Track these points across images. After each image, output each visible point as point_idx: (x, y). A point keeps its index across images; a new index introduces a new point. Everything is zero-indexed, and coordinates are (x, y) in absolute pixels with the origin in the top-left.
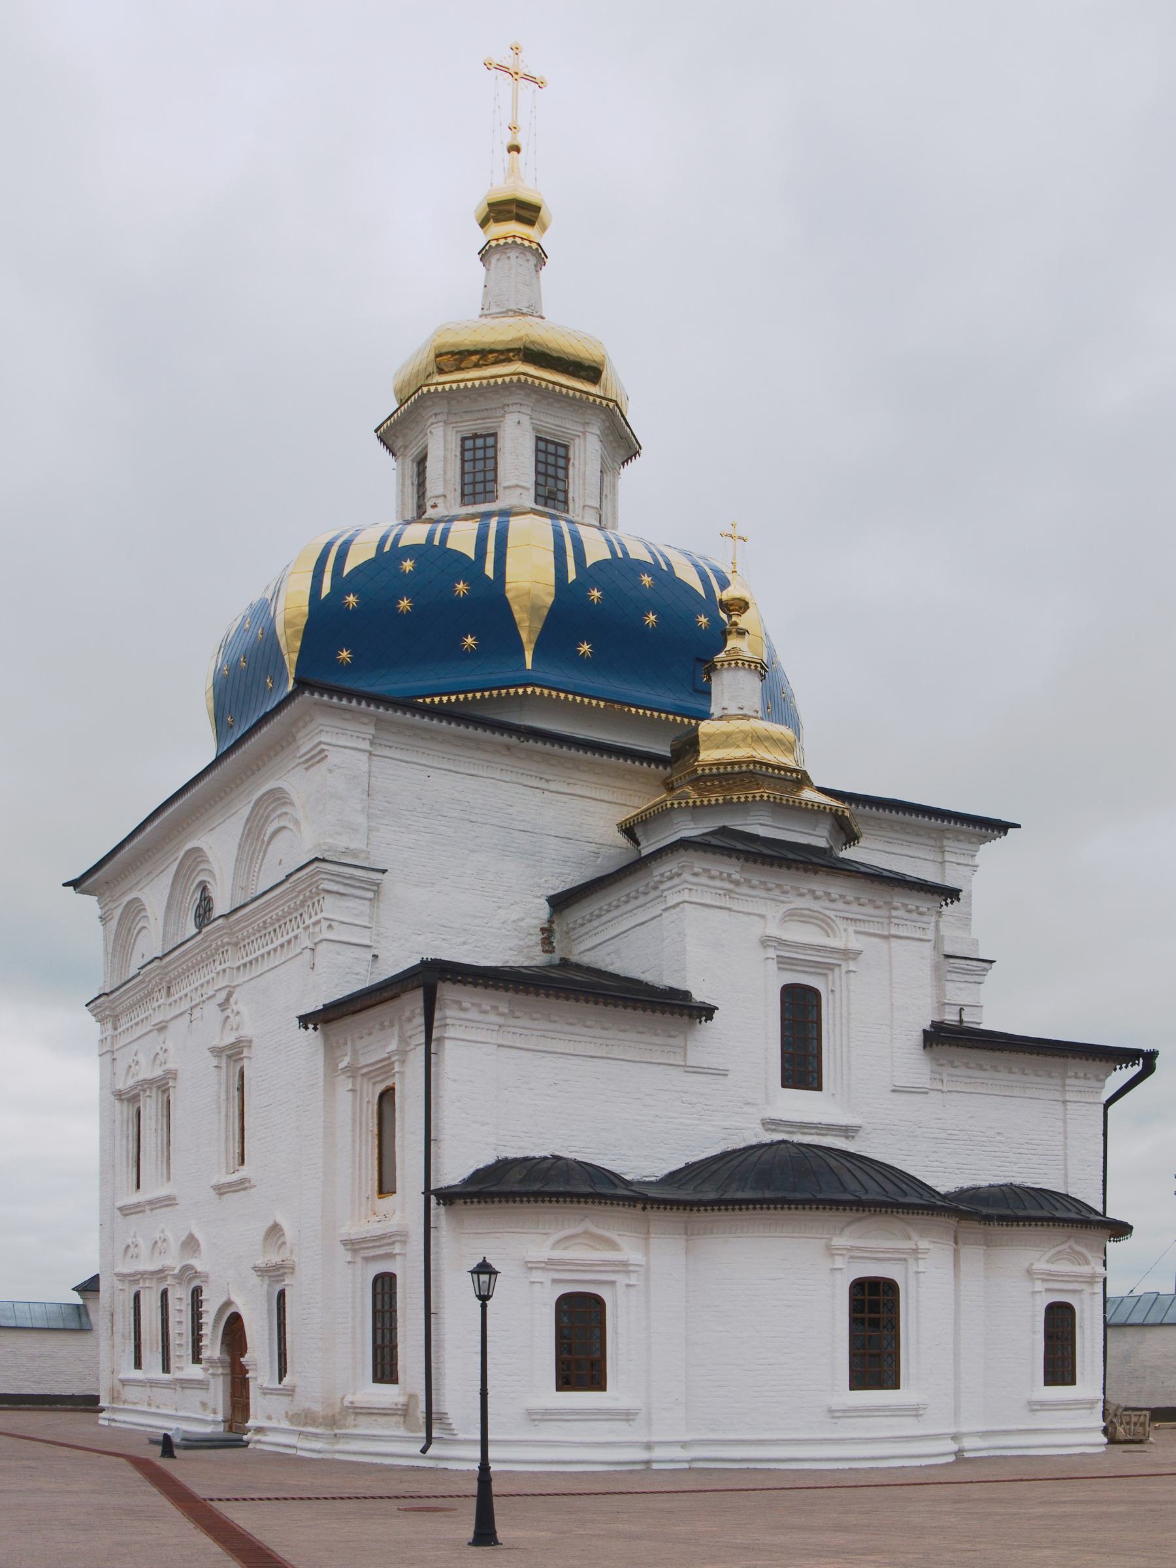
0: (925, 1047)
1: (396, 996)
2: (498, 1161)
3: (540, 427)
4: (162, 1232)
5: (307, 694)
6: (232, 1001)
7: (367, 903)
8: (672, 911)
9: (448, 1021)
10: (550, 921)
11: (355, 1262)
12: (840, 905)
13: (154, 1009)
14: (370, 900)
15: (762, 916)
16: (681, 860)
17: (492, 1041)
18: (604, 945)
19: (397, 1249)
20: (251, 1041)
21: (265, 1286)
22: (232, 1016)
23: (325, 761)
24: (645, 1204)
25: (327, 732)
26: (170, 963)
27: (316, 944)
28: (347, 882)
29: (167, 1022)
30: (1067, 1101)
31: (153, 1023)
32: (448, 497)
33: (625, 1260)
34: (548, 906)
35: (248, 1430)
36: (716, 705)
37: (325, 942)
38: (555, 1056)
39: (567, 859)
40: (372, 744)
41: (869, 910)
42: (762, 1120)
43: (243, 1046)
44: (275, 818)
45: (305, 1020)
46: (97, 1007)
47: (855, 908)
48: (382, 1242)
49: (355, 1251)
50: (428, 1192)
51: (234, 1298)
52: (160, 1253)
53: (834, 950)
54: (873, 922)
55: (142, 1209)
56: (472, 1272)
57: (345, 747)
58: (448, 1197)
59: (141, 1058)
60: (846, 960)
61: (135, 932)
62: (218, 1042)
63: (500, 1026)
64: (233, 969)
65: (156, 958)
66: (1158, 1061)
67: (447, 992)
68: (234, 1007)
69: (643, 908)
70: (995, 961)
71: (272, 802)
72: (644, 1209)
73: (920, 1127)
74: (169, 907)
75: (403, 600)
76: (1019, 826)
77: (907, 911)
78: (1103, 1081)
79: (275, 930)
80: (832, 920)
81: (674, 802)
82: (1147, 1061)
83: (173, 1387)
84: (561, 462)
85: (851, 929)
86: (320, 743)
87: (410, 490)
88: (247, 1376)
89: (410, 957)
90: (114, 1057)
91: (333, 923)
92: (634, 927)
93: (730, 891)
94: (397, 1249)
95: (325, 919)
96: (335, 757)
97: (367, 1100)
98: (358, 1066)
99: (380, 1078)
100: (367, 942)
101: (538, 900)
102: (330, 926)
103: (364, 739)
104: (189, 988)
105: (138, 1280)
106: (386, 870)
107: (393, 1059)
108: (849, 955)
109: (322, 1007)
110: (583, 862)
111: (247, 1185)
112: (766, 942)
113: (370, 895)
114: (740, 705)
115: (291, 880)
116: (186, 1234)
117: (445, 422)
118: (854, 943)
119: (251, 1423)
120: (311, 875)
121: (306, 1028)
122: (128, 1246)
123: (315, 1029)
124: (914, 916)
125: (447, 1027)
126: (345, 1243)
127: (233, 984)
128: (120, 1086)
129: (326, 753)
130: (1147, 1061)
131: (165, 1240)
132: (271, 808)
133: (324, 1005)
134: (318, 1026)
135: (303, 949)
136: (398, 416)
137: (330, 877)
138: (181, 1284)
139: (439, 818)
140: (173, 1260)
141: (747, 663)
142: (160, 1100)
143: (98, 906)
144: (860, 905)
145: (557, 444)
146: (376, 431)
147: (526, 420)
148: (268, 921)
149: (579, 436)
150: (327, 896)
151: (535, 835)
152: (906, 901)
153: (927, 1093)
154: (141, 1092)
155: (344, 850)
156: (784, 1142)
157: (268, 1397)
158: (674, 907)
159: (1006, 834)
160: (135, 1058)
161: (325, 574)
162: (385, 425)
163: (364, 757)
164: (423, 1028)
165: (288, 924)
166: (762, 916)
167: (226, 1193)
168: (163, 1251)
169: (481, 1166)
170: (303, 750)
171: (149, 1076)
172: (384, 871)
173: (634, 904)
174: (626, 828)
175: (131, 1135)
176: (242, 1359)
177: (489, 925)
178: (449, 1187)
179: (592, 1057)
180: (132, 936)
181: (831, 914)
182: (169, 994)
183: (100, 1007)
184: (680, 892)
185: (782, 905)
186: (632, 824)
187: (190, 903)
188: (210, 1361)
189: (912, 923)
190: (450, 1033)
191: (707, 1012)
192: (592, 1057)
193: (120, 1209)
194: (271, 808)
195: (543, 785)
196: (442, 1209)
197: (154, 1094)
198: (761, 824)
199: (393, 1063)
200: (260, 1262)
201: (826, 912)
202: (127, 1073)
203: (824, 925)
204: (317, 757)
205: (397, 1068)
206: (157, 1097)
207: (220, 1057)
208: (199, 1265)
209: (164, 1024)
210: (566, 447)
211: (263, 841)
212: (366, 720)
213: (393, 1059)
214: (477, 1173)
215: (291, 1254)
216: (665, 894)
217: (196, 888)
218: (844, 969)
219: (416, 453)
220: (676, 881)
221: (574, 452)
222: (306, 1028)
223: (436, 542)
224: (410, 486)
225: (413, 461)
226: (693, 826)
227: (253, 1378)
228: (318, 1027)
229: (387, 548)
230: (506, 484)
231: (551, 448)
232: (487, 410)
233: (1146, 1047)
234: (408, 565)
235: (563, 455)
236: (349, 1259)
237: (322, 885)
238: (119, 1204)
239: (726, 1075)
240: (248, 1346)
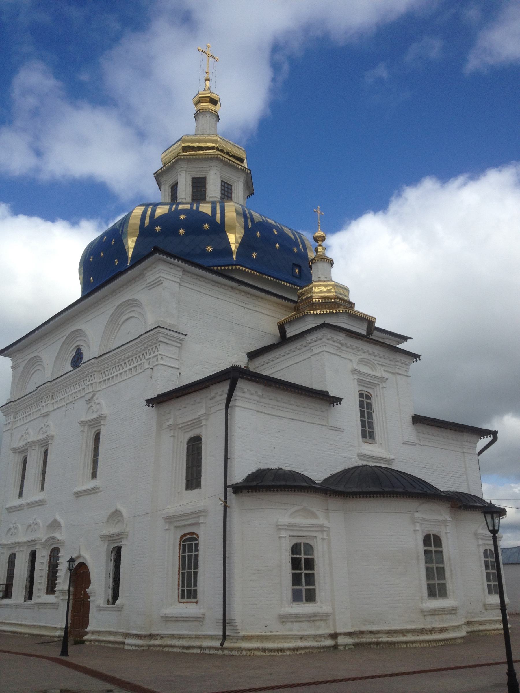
0: (413, 424)
1: (208, 387)
2: (258, 470)
3: (223, 177)
4: (35, 520)
5: (157, 254)
6: (95, 398)
7: (178, 348)
8: (317, 356)
9: (237, 398)
10: (248, 364)
11: (170, 529)
12: (377, 358)
13: (43, 406)
14: (179, 347)
15: (351, 360)
16: (322, 333)
17: (254, 409)
18: (275, 373)
19: (202, 520)
20: (105, 417)
21: (106, 546)
22: (94, 405)
23: (161, 285)
25: (163, 272)
26: (56, 384)
27: (154, 366)
28: (170, 338)
29: (50, 412)
30: (465, 452)
31: (41, 413)
32: (186, 199)
33: (322, 524)
34: (247, 357)
35: (87, 633)
36: (315, 277)
37: (160, 365)
38: (279, 418)
39: (253, 338)
40: (180, 280)
41: (387, 361)
42: (358, 454)
43: (102, 419)
44: (127, 313)
45: (149, 402)
46: (6, 408)
47: (382, 360)
48: (190, 517)
49: (170, 523)
50: (226, 487)
51: (83, 554)
52: (32, 532)
53: (377, 378)
54: (389, 367)
55: (23, 508)
56: (68, 561)
57: (170, 280)
58: (238, 489)
59: (31, 431)
60: (381, 382)
61: (32, 373)
62: (84, 419)
63: (257, 402)
64: (97, 383)
65: (49, 381)
66: (498, 435)
67: (241, 384)
68: (97, 401)
69: (298, 356)
71: (126, 306)
73: (415, 461)
74: (56, 359)
75: (181, 230)
76: (411, 338)
77: (401, 363)
78: (476, 444)
79: (125, 363)
80: (376, 365)
81: (298, 315)
83: (33, 608)
84: (229, 191)
85: (382, 369)
86: (160, 277)
87: (168, 197)
88: (89, 600)
89: (193, 375)
90: (13, 432)
91: (163, 357)
92: (294, 364)
93: (340, 348)
94: (202, 520)
95: (160, 354)
96: (166, 283)
97: (180, 441)
98: (177, 424)
99: (189, 430)
100: (177, 366)
101: (243, 354)
102: (162, 358)
103: (177, 278)
104: (66, 395)
105: (15, 547)
106: (187, 335)
107: (201, 418)
108: (383, 380)
109: (157, 396)
110: (259, 339)
111: (97, 490)
112: (354, 371)
113: (179, 345)
114: (326, 276)
115: (141, 338)
116: (53, 519)
117: (186, 171)
118: (386, 375)
119: (89, 629)
120: (154, 335)
121: (149, 406)
122: (10, 529)
123: (153, 406)
124: (404, 365)
125: (236, 401)
126: (165, 518)
127: (96, 390)
128: (15, 446)
129: (162, 281)
131: (36, 524)
132: (125, 309)
133: (158, 395)
134: (154, 405)
135: (145, 370)
136: (163, 169)
137: (163, 335)
138: (45, 548)
139: (205, 315)
140: (42, 535)
141: (328, 260)
142: (40, 451)
143: (11, 362)
144: (385, 359)
145: (228, 184)
146: (154, 174)
147: (218, 173)
148: (117, 361)
149: (236, 182)
150: (161, 344)
151: (242, 326)
152: (401, 359)
153: (415, 445)
154: (29, 448)
155: (169, 324)
156: (366, 465)
157: (102, 612)
158: (318, 354)
159: (406, 341)
160: (26, 431)
161: (146, 217)
162: (159, 171)
163: (177, 285)
164: (225, 401)
165: (92, 376)
166: (351, 360)
167: (81, 496)
168: (34, 530)
169: (250, 472)
170: (149, 281)
171: (35, 439)
172: (186, 335)
173: (293, 354)
174: (280, 325)
175: (18, 471)
176: (87, 590)
177: (224, 363)
178: (237, 484)
179: (293, 419)
180: (30, 374)
181: (375, 362)
182: (52, 399)
183: (8, 408)
184: (320, 347)
185: (358, 356)
186: (283, 323)
187: (69, 356)
188: (62, 592)
189: (403, 369)
190: (238, 403)
191: (338, 400)
192: (293, 419)
193: (8, 509)
194: (125, 309)
195: (244, 305)
196: (233, 496)
197: (37, 448)
198: (344, 323)
199: (201, 420)
200: (104, 532)
201: (374, 361)
202: (20, 439)
203: (371, 366)
204: (158, 283)
205: (204, 423)
206: (38, 450)
207: (84, 426)
208: (58, 536)
209: (48, 413)
210: (231, 186)
211: (118, 324)
212: (179, 269)
213: (201, 418)
214: (249, 476)
215: (126, 527)
216: (312, 348)
217: (74, 349)
218: (381, 386)
219: (171, 183)
220: (319, 342)
221: (234, 188)
224: (168, 196)
225: (169, 186)
226: (314, 323)
227: (92, 601)
228: (154, 405)
230: (211, 196)
231: (226, 185)
232: (202, 168)
235: (230, 188)
236: (167, 528)
237: (160, 339)
238: (8, 506)
239: (343, 431)
240: (92, 582)
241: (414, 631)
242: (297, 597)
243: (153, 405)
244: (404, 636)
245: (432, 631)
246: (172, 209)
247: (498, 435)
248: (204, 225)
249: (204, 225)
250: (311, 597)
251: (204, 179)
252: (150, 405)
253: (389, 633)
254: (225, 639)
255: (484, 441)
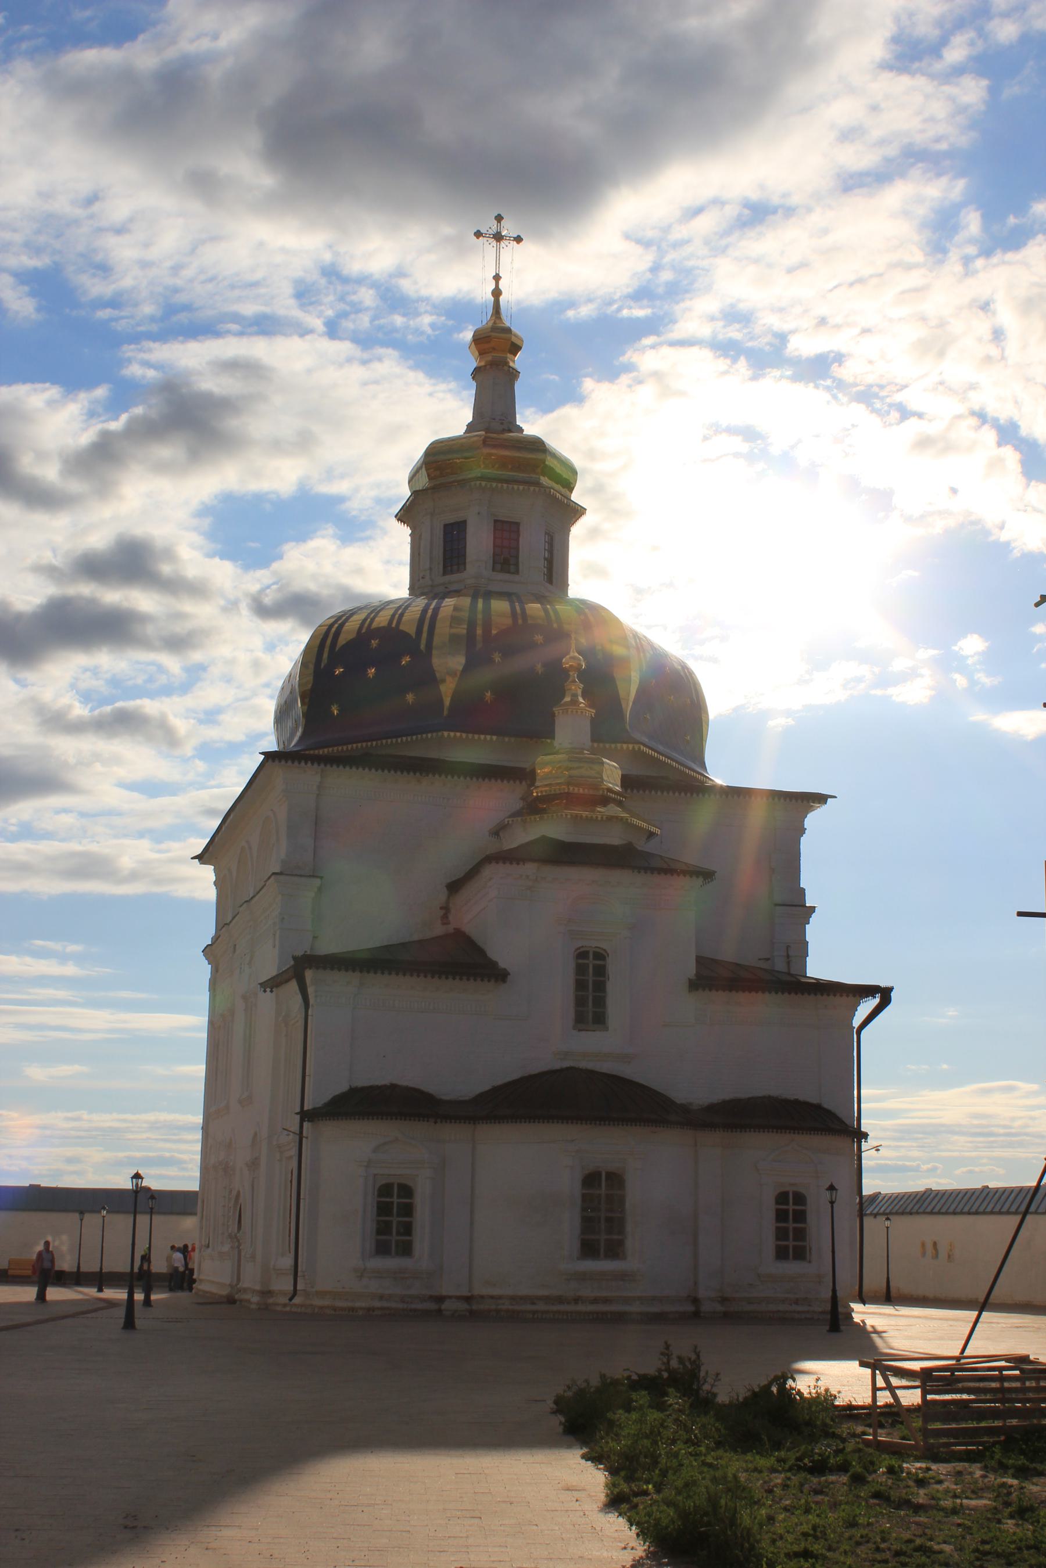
24: (272, 989)
70: (821, 799)
72: (436, 1123)
82: (885, 995)
121: (265, 991)
123: (271, 991)
130: (885, 995)
134: (274, 990)
141: (587, 712)
222: (265, 991)
223: (394, 625)
228: (274, 990)
229: (364, 631)
233: (883, 984)
234: (374, 643)
241: (547, 1299)
242: (782, 1254)
243: (272, 989)
244: (533, 1303)
245: (577, 1300)
246: (362, 630)
247: (892, 994)
248: (409, 656)
249: (409, 656)
250: (800, 1254)
251: (464, 522)
252: (267, 989)
253: (513, 1299)
254: (296, 1294)
255: (873, 1003)
